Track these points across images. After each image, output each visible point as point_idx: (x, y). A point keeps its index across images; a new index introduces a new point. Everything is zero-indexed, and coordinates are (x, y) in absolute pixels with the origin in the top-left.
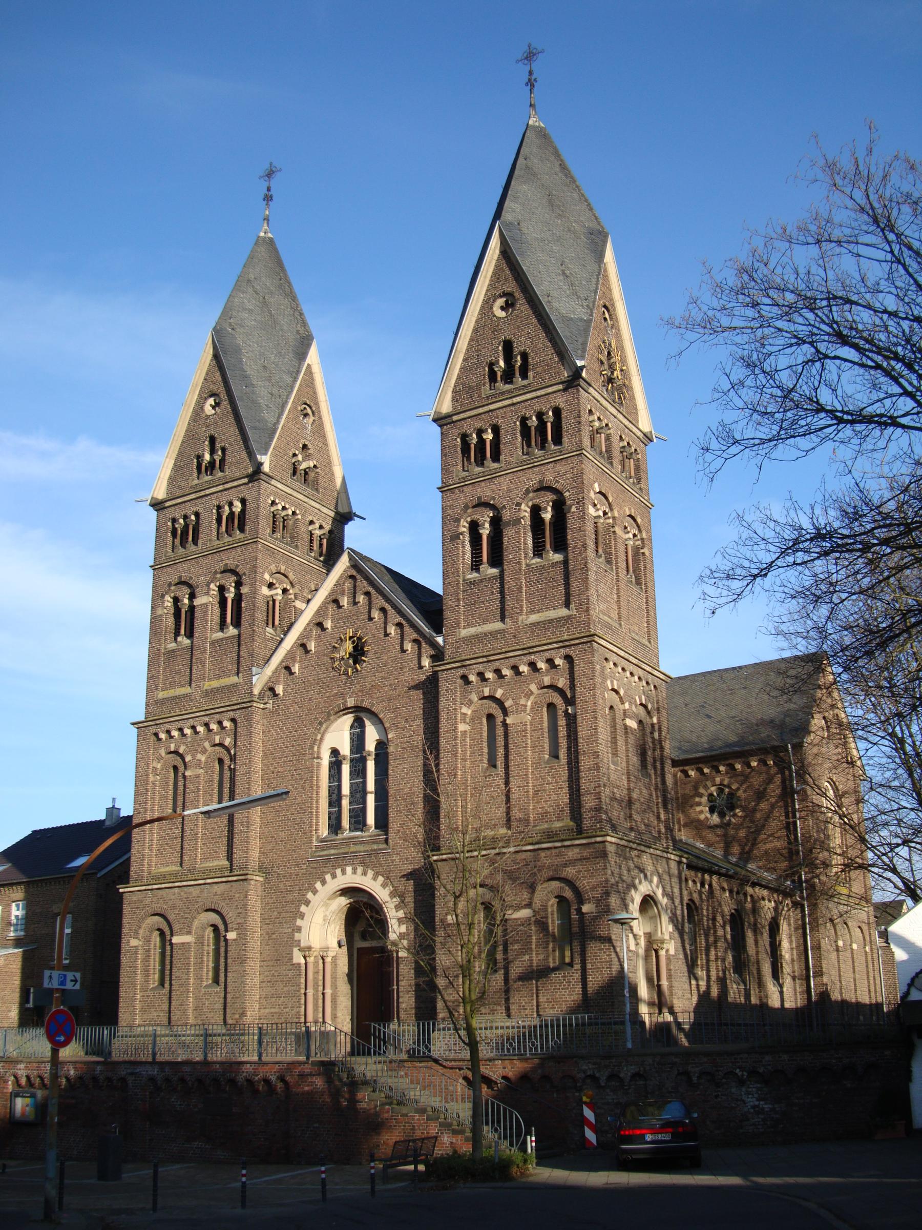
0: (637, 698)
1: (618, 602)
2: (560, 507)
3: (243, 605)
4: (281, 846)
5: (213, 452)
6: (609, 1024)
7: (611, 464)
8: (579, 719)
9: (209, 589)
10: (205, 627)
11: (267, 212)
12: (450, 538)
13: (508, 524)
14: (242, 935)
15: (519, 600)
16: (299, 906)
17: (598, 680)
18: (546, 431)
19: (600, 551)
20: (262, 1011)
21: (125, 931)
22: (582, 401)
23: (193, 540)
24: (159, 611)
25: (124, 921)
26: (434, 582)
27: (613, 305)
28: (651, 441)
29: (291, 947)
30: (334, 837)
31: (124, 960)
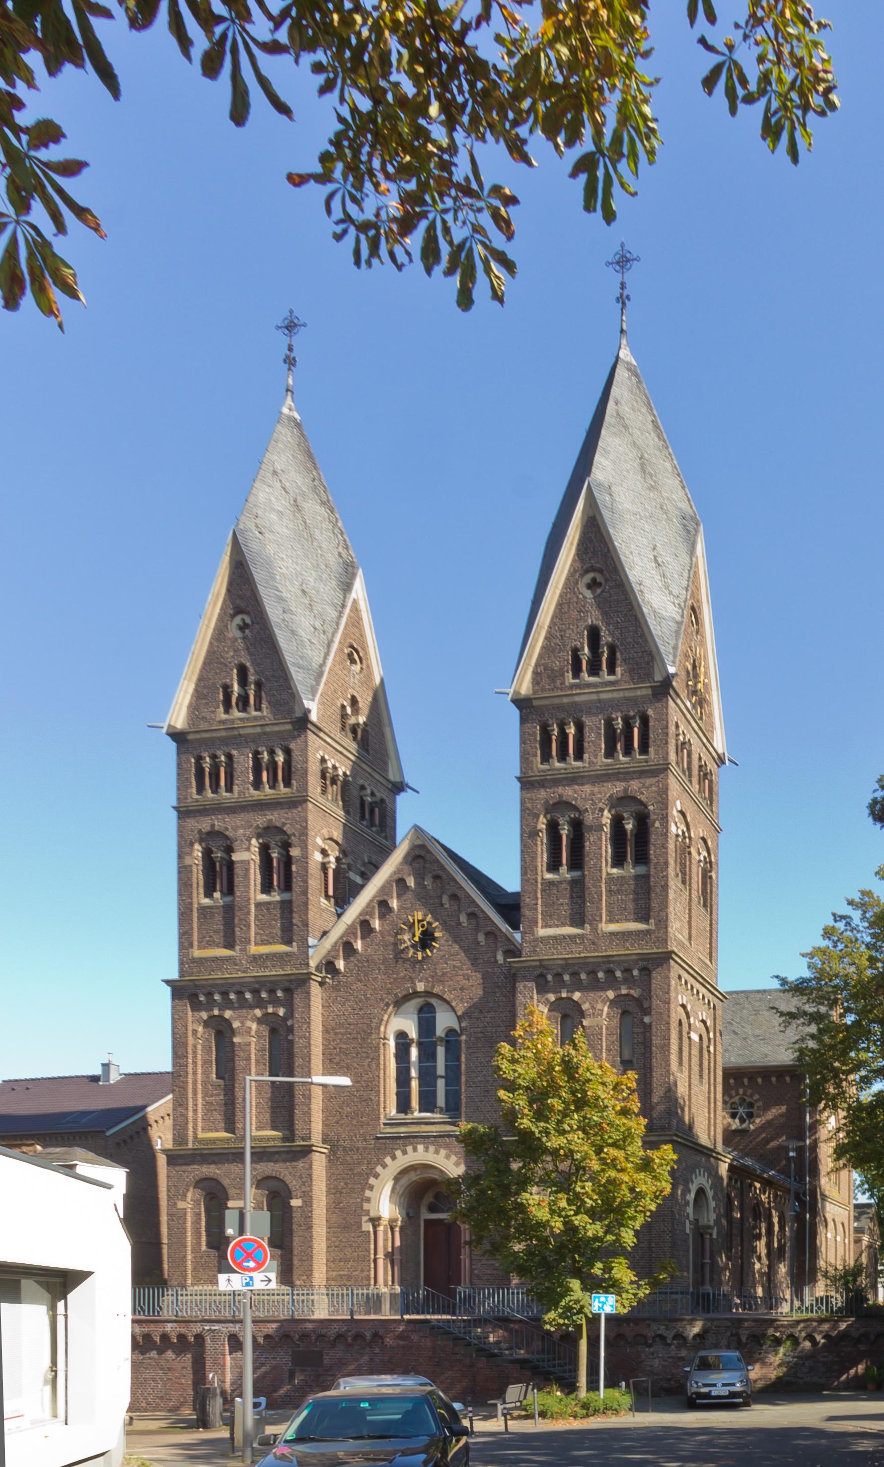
2: (643, 820)
3: (294, 868)
4: (346, 1121)
7: (690, 781)
8: (654, 1029)
9: (250, 844)
10: (248, 886)
11: (290, 382)
12: (528, 835)
13: (590, 828)
16: (368, 1178)
17: (673, 994)
22: (671, 711)
24: (188, 861)
26: (511, 882)
28: (723, 763)
29: (360, 1216)
30: (402, 1116)
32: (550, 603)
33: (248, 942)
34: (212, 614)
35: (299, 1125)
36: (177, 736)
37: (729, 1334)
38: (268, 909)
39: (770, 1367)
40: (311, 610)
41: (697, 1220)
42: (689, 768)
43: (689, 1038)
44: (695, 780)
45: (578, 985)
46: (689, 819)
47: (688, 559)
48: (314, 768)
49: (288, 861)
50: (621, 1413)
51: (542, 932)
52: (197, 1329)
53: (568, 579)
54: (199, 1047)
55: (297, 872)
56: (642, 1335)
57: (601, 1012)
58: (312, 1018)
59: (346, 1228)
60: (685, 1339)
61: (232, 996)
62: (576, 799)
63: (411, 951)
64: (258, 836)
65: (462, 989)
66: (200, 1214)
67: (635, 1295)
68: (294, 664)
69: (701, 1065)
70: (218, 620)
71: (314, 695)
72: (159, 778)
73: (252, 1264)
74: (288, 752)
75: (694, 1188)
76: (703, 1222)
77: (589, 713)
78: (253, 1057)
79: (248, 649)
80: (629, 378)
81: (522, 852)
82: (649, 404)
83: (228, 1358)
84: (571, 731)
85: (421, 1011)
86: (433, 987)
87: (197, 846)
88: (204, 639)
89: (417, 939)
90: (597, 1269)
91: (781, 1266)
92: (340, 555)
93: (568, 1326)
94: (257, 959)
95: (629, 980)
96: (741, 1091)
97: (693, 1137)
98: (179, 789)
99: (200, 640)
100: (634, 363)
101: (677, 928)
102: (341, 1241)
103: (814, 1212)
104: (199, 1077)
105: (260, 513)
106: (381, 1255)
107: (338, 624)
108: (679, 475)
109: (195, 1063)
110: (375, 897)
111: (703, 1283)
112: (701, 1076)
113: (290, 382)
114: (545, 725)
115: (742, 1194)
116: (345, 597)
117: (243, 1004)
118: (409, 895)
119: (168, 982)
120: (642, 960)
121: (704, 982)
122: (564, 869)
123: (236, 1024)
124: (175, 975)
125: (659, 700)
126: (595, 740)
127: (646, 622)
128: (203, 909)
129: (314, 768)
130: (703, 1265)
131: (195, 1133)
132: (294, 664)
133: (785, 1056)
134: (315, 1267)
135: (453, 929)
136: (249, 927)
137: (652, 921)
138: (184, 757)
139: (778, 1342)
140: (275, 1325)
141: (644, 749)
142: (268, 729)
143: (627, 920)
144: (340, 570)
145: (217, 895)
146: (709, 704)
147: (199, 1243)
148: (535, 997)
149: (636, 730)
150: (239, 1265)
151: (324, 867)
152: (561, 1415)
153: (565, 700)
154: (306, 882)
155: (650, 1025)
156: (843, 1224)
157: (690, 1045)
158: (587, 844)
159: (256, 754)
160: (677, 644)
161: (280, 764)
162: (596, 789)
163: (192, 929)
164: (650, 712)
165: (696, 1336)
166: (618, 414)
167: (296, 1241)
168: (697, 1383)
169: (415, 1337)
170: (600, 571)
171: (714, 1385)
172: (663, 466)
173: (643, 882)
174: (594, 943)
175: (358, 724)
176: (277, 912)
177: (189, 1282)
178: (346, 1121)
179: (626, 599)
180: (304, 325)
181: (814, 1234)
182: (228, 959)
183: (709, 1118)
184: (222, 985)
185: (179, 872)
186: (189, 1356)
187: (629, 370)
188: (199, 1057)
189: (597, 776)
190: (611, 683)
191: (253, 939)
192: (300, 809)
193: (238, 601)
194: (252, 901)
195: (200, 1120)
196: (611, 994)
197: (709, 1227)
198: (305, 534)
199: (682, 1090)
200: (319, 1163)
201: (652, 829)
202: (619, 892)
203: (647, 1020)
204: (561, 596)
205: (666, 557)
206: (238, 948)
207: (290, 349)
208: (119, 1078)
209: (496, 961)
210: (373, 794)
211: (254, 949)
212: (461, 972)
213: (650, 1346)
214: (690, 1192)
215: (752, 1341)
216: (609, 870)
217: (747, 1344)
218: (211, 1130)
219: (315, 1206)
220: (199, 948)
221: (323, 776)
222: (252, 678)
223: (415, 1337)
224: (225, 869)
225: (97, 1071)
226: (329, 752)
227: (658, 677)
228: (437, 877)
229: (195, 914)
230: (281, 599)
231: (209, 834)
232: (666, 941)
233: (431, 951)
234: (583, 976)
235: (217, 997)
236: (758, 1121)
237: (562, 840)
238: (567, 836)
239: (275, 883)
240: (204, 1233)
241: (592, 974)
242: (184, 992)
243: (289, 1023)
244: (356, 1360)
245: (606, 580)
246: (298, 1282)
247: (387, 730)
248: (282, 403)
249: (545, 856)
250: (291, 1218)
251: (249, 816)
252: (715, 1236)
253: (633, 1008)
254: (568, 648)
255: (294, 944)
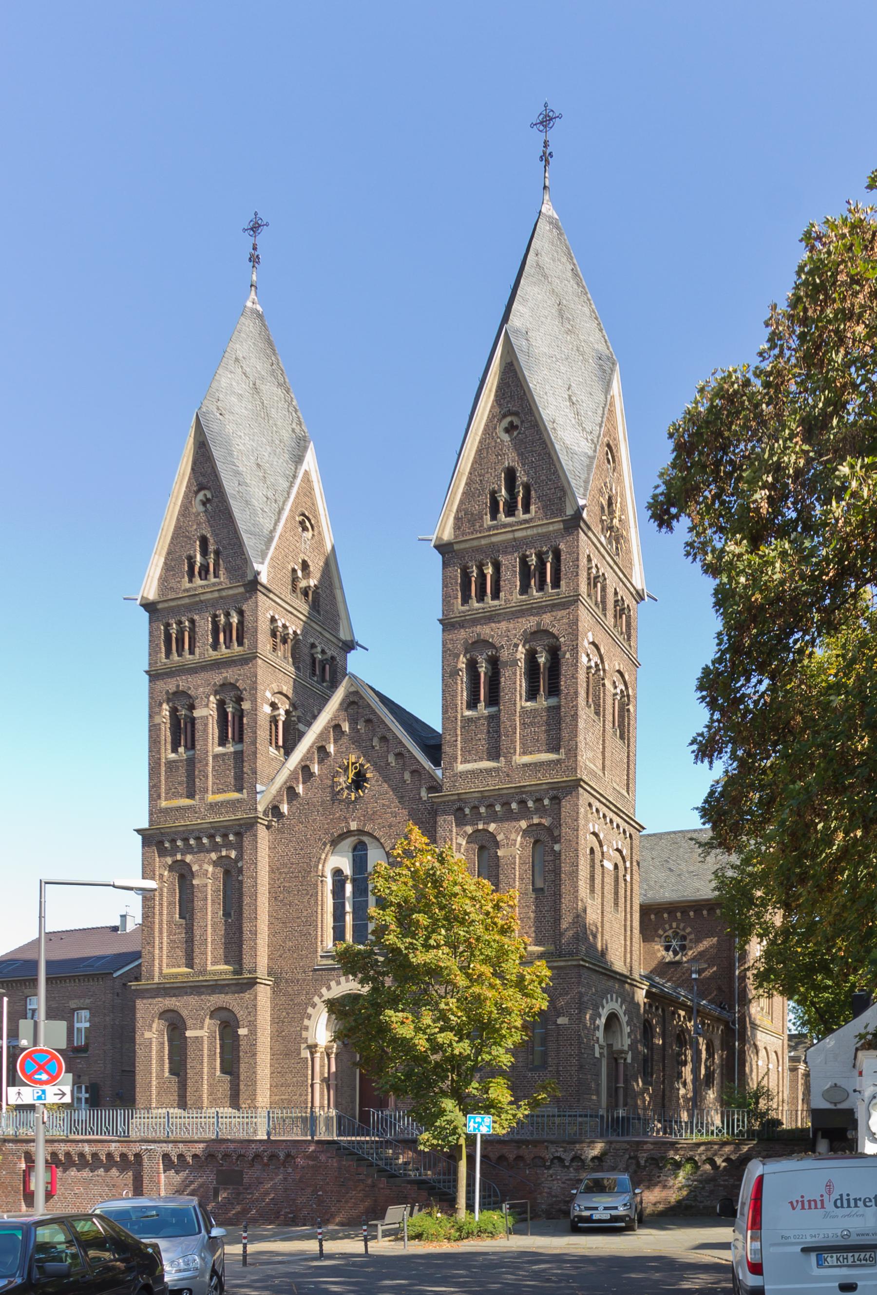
0: (614, 843)
1: (603, 753)
2: (555, 653)
5: (204, 553)
6: (575, 1116)
7: (605, 615)
8: (563, 857)
9: (209, 700)
10: (206, 740)
11: (254, 278)
12: (449, 674)
14: (253, 1032)
15: (513, 742)
16: (306, 1008)
17: (582, 822)
18: (545, 573)
19: (590, 700)
20: (274, 1097)
21: (139, 1023)
22: (581, 543)
23: (190, 648)
24: (157, 720)
25: (138, 1015)
26: (434, 720)
27: (616, 445)
28: (643, 599)
31: (140, 1052)
32: (470, 450)
33: (206, 791)
34: (178, 492)
35: (246, 959)
36: (149, 606)
37: (627, 1156)
38: (223, 760)
39: (674, 1188)
40: (265, 482)
41: (610, 1046)
42: (604, 602)
43: (602, 866)
44: (610, 613)
45: (493, 817)
46: (602, 651)
47: (603, 397)
48: (264, 627)
49: (240, 714)
50: (499, 1238)
51: (461, 767)
52: (136, 1148)
53: (487, 425)
54: (165, 890)
55: (248, 724)
56: (540, 1158)
57: (514, 844)
58: (259, 859)
59: (287, 1055)
60: (583, 1161)
61: (192, 842)
62: (493, 637)
63: (346, 792)
64: (216, 693)
65: (390, 826)
66: (163, 1043)
67: (514, 1116)
68: (246, 531)
69: (616, 893)
70: (184, 497)
71: (264, 559)
72: (133, 643)
73: (44, 1077)
74: (241, 613)
75: (604, 1013)
76: (617, 1046)
77: (505, 553)
78: (209, 897)
79: (209, 521)
80: (551, 231)
81: (443, 691)
82: (570, 254)
83: (162, 1176)
84: (489, 571)
85: (355, 849)
86: (365, 825)
87: (165, 706)
88: (171, 516)
89: (350, 781)
90: (473, 1089)
91: (710, 1092)
92: (293, 430)
93: (443, 1147)
94: (212, 806)
95: (541, 810)
96: (674, 925)
97: (606, 963)
98: (150, 655)
99: (168, 517)
100: (556, 216)
101: (588, 759)
102: (283, 1067)
103: (743, 1039)
104: (165, 917)
105: (221, 396)
106: (317, 1080)
107: (289, 493)
108: (596, 318)
109: (161, 904)
110: (314, 743)
111: (617, 1106)
112: (616, 904)
113: (254, 278)
114: (467, 568)
115: (664, 1023)
116: (296, 469)
117: (201, 849)
118: (345, 740)
119: (138, 831)
120: (552, 789)
121: (618, 812)
122: (481, 705)
123: (195, 868)
124: (145, 825)
125: (570, 534)
126: (511, 578)
127: (558, 458)
128: (170, 764)
129: (264, 627)
130: (617, 1089)
131: (161, 969)
132: (246, 531)
133: (704, 888)
134: (258, 1091)
135: (382, 769)
136: (207, 777)
137: (562, 750)
138: (154, 625)
139: (678, 1166)
140: (202, 1145)
141: (556, 584)
142: (224, 593)
143: (539, 751)
144: (293, 444)
145: (181, 750)
146: (627, 541)
147: (163, 1070)
148: (454, 831)
149: (548, 565)
150: (30, 1077)
151: (274, 720)
152: (436, 1237)
153: (483, 542)
154: (256, 733)
155: (560, 853)
156: (776, 1052)
157: (603, 873)
158: (503, 679)
159: (215, 616)
160: (588, 478)
161: (235, 625)
162: (511, 626)
163: (160, 781)
164: (562, 546)
165: (594, 1158)
166: (538, 265)
167: (243, 1067)
168: (579, 1206)
169: (323, 1158)
170: (516, 414)
171: (596, 1209)
172: (582, 312)
173: (554, 712)
174: (508, 776)
175: (309, 587)
176: (231, 762)
177: (154, 1105)
178: (288, 954)
179: (540, 438)
180: (267, 225)
181: (743, 1062)
182: (189, 808)
183: (625, 945)
184: (184, 832)
185: (150, 731)
186: (130, 1174)
187: (551, 223)
188: (165, 899)
189: (512, 613)
190: (526, 521)
191: (210, 788)
192: (250, 665)
193: (200, 479)
194: (210, 754)
195: (165, 957)
196: (524, 824)
197: (622, 1052)
198: (263, 413)
199: (592, 916)
200: (264, 994)
201: (563, 661)
202: (532, 724)
203: (557, 847)
204: (480, 442)
205: (581, 395)
206: (197, 797)
207: (255, 249)
208: (135, 927)
209: (421, 798)
210: (323, 652)
211: (211, 798)
212: (390, 810)
213: (549, 1168)
214: (600, 1016)
215: (649, 1167)
216: (523, 703)
217: (645, 1167)
218: (173, 966)
219: (259, 1035)
220: (166, 799)
221: (274, 634)
222: (212, 548)
223: (323, 1158)
224: (189, 726)
225: (117, 922)
226: (280, 611)
227: (570, 512)
228: (368, 721)
229: (163, 769)
230: (237, 473)
231: (175, 693)
232: (576, 769)
233: (363, 792)
234: (498, 808)
235: (179, 843)
236: (690, 953)
237: (482, 681)
238: (485, 674)
239: (230, 736)
240: (167, 1061)
241: (506, 804)
242: (153, 839)
243: (240, 865)
244: (272, 1179)
245: (522, 422)
246: (243, 1106)
247: (338, 592)
248: (247, 298)
249: (465, 694)
250: (239, 1046)
251: (203, 675)
252: (629, 1060)
253: (544, 837)
254: (487, 491)
255: (245, 791)
